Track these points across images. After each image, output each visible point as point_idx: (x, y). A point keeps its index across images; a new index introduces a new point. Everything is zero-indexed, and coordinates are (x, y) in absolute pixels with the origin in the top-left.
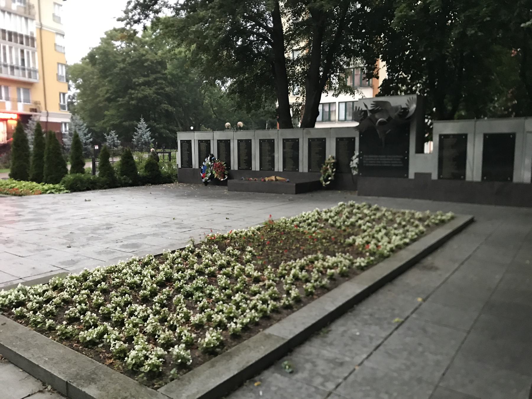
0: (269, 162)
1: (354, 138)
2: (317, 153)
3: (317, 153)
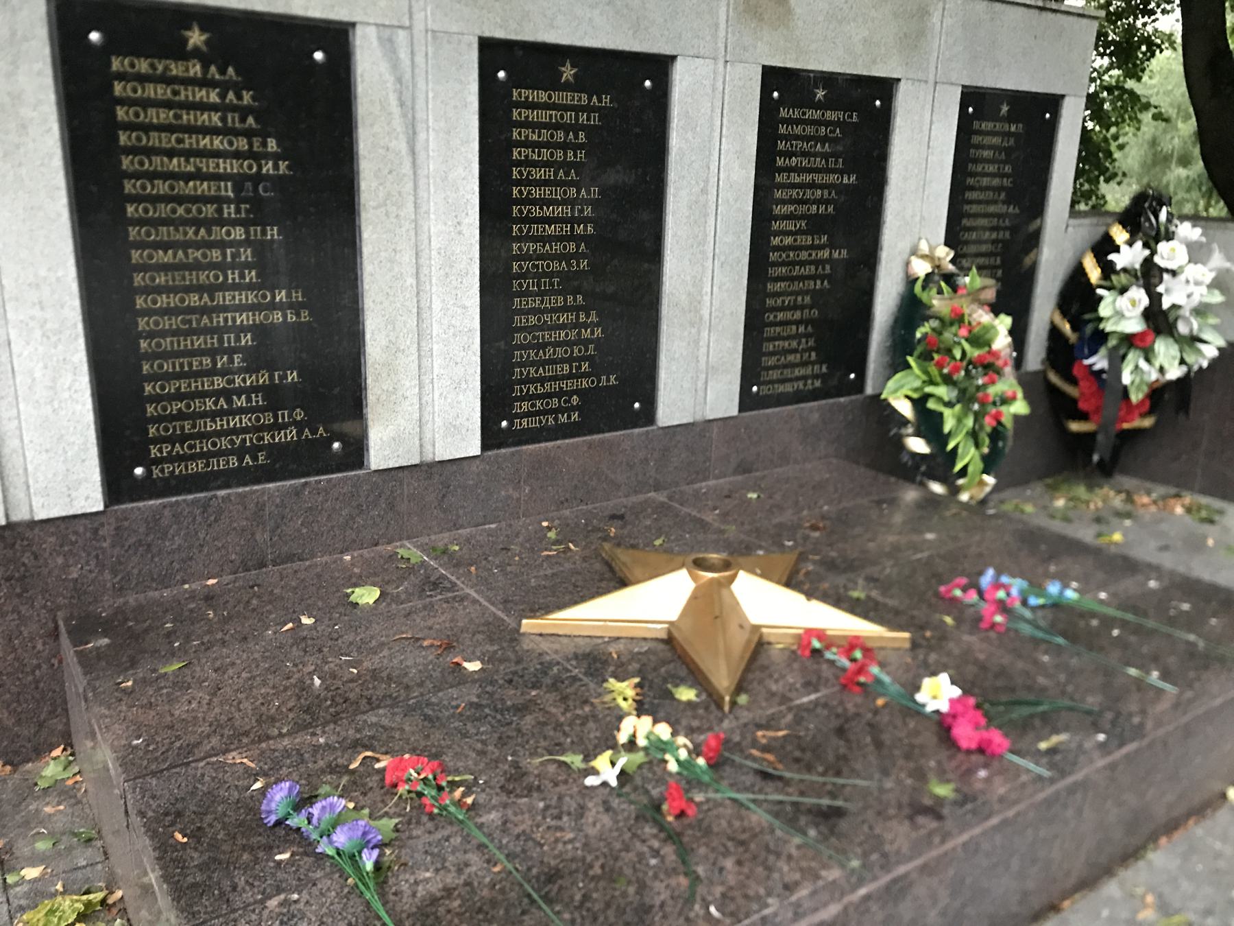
0: (256, 360)
1: (1053, 102)
2: (816, 225)
3: (816, 225)
